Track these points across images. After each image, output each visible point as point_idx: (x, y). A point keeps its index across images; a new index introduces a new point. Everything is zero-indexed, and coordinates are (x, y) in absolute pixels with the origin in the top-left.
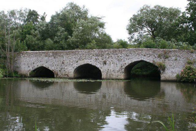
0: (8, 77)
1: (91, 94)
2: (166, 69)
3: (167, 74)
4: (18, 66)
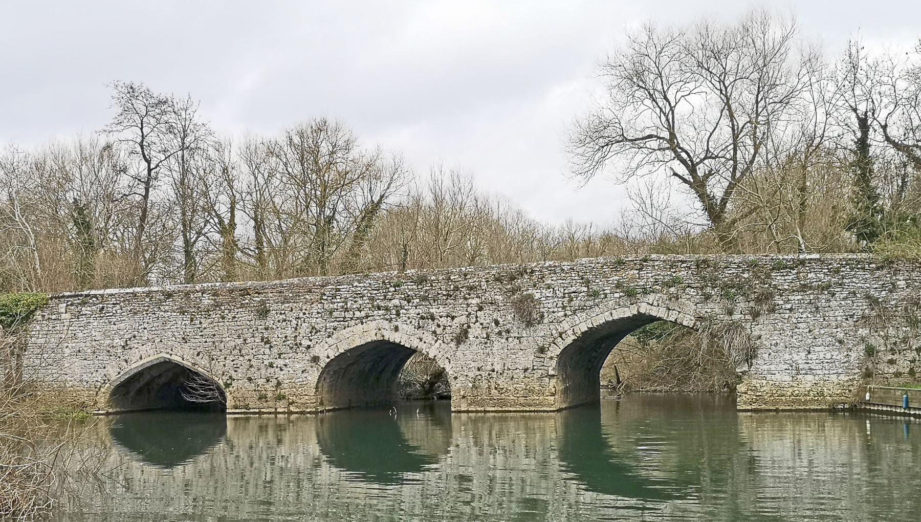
0: (507, 417)
1: (401, 481)
2: (763, 354)
3: (769, 377)
4: (365, 161)
